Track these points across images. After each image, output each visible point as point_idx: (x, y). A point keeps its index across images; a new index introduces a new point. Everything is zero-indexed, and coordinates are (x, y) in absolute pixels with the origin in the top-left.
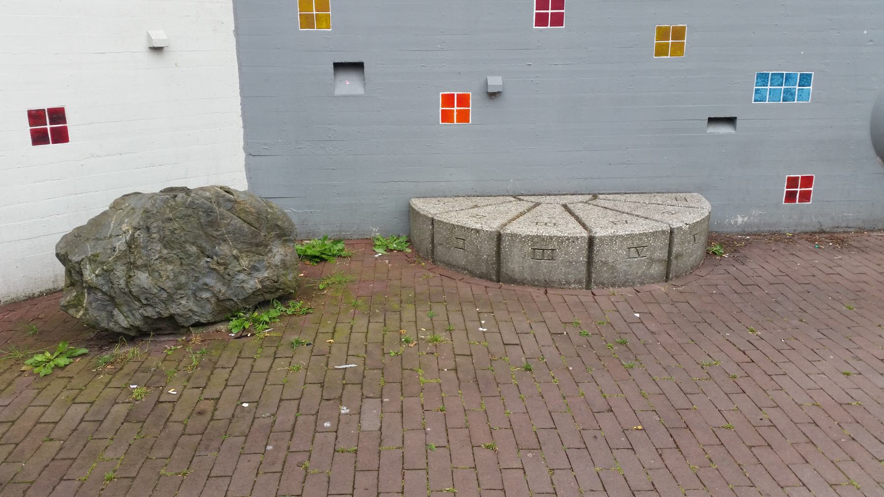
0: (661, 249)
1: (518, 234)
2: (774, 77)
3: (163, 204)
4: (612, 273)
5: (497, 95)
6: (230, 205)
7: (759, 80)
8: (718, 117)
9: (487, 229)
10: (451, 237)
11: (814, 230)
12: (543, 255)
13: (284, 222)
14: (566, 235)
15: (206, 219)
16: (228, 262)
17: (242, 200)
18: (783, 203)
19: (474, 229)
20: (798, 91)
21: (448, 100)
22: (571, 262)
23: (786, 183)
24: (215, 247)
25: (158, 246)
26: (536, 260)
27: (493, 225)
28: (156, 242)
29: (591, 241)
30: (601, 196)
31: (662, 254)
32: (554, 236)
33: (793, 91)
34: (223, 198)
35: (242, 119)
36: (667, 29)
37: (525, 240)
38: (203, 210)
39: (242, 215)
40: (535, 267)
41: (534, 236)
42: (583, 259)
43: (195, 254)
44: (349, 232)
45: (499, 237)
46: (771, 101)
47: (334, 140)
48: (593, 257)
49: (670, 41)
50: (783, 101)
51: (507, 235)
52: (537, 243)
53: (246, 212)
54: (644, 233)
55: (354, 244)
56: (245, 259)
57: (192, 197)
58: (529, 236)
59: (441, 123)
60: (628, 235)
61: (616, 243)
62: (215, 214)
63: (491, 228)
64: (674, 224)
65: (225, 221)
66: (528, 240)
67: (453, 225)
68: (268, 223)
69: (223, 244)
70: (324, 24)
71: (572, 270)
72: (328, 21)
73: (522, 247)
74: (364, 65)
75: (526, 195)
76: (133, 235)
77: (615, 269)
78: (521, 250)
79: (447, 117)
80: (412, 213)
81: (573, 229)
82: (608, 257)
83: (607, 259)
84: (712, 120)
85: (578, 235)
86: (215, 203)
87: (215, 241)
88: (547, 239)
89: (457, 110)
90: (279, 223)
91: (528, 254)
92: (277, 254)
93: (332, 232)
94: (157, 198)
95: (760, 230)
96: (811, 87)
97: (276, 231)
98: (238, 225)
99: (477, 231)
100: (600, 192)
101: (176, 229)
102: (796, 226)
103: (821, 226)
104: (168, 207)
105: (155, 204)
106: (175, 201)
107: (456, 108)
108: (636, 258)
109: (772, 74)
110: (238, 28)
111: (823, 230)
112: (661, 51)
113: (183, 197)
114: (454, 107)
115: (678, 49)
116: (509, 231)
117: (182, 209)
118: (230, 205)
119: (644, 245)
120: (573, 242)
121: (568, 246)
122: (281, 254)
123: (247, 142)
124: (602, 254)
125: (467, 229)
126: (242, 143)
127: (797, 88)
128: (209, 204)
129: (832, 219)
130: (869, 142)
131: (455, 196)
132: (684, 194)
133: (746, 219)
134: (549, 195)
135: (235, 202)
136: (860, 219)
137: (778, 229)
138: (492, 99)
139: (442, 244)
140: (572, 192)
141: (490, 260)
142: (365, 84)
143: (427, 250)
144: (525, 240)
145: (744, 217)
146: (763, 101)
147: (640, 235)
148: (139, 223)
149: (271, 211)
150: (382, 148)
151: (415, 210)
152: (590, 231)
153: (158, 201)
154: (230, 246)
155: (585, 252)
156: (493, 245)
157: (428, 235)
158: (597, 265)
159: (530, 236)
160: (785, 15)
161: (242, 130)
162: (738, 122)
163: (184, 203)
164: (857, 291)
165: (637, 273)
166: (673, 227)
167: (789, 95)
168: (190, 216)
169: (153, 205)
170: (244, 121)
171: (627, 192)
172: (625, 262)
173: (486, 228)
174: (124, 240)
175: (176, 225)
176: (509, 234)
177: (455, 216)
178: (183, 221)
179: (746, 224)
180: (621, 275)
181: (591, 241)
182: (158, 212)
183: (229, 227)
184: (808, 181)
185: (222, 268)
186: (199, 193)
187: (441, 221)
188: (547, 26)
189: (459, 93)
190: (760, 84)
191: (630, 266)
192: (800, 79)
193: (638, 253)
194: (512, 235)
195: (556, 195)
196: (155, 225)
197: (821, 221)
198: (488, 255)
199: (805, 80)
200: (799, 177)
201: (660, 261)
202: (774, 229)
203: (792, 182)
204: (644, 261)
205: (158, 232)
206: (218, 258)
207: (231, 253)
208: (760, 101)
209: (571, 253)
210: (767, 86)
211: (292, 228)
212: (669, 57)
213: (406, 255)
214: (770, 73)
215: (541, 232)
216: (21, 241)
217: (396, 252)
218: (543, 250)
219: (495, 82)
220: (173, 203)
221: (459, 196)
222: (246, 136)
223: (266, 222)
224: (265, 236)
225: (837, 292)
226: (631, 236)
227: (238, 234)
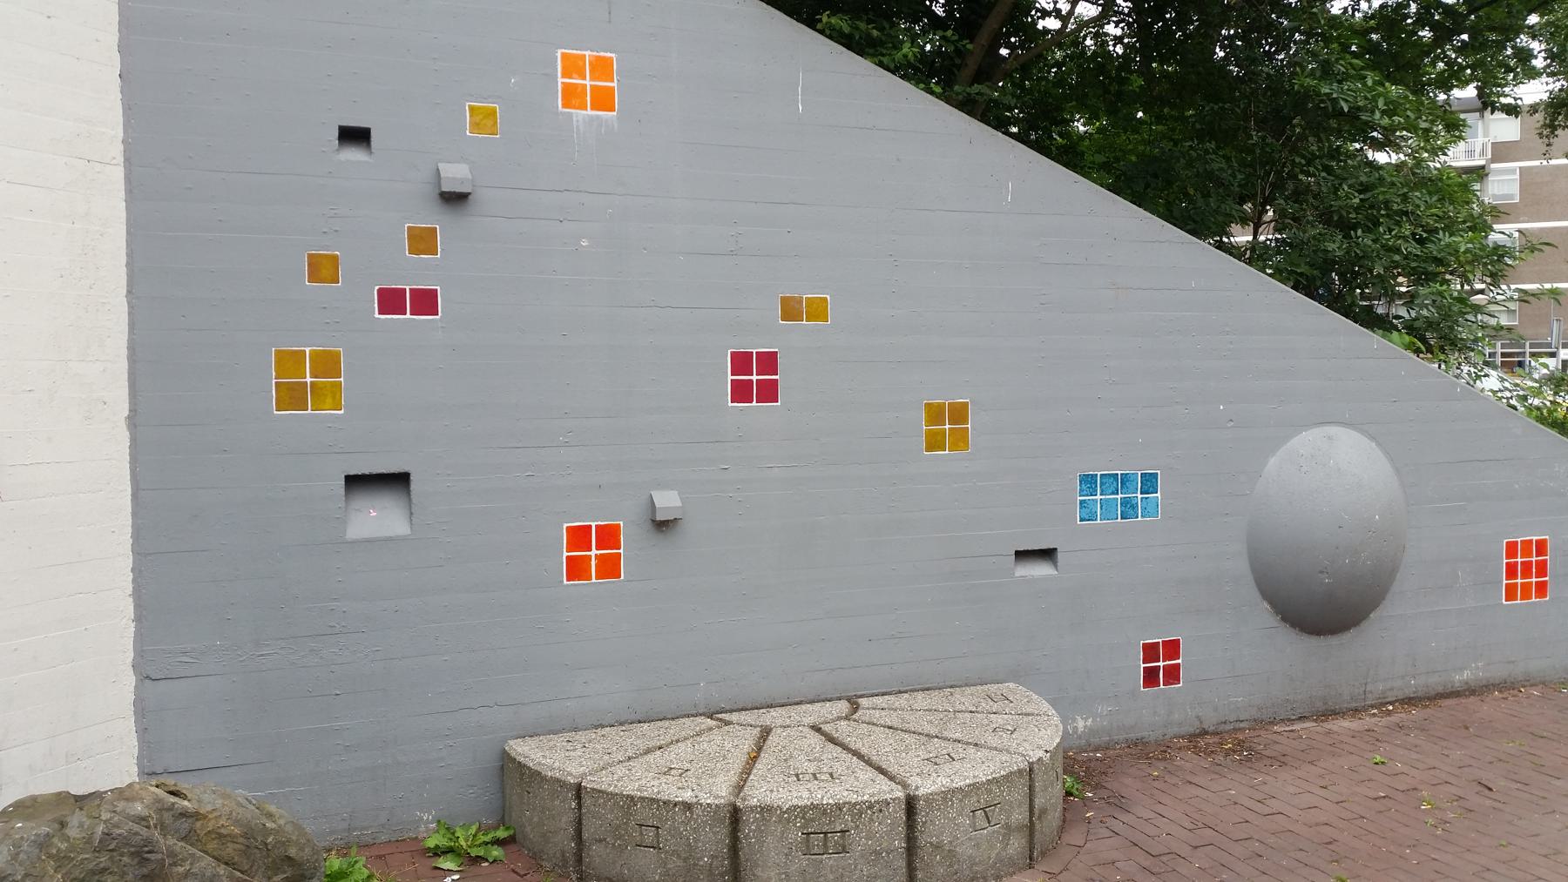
0: (1020, 806)
1: (775, 805)
2: (1104, 480)
3: (38, 850)
4: (951, 866)
5: (671, 525)
6: (184, 825)
7: (1083, 485)
8: (1030, 549)
9: (709, 801)
10: (625, 823)
11: (1191, 730)
12: (825, 845)
13: (302, 849)
14: (865, 798)
15: (137, 872)
17: (209, 808)
18: (1142, 689)
19: (679, 802)
20: (1142, 501)
21: (579, 537)
22: (878, 853)
23: (1142, 653)
26: (813, 857)
27: (717, 791)
29: (911, 805)
30: (864, 702)
31: (1019, 816)
32: (845, 803)
33: (1133, 502)
34: (172, 813)
35: (134, 601)
36: (941, 407)
37: (790, 818)
38: (133, 849)
39: (211, 846)
40: (811, 871)
41: (805, 807)
42: (899, 844)
44: (366, 828)
45: (735, 815)
46: (1104, 519)
47: (341, 633)
48: (916, 838)
49: (947, 426)
50: (1122, 519)
51: (753, 809)
52: (813, 820)
53: (220, 836)
54: (994, 778)
55: (384, 856)
57: (105, 822)
58: (796, 807)
59: (565, 582)
60: (969, 785)
61: (952, 804)
62: (159, 856)
63: (717, 797)
64: (1031, 753)
65: (181, 869)
66: (796, 817)
67: (632, 798)
68: (269, 856)
70: (329, 400)
71: (882, 869)
72: (338, 397)
73: (783, 833)
74: (411, 478)
75: (731, 711)
77: (954, 856)
78: (782, 837)
79: (576, 569)
80: (511, 772)
81: (864, 786)
82: (942, 833)
83: (941, 838)
84: (1022, 555)
85: (888, 796)
86: (156, 827)
88: (831, 811)
89: (596, 555)
90: (292, 852)
91: (796, 846)
93: (332, 832)
94: (22, 838)
95: (1113, 740)
96: (1159, 495)
97: (285, 872)
98: (208, 874)
99: (688, 806)
100: (859, 693)
102: (1166, 727)
103: (1201, 722)
104: (50, 856)
105: (18, 854)
106: (67, 839)
107: (594, 552)
108: (984, 829)
109: (1101, 475)
110: (136, 411)
111: (1204, 729)
112: (934, 443)
113: (81, 825)
114: (591, 550)
115: (960, 440)
116: (755, 800)
117: (87, 856)
119: (995, 802)
120: (881, 811)
121: (871, 820)
123: (143, 651)
124: (933, 828)
125: (665, 803)
126: (130, 656)
127: (1140, 496)
128: (144, 832)
129: (1216, 710)
130: (1249, 579)
131: (596, 727)
132: (996, 686)
133: (1089, 722)
134: (771, 706)
135: (197, 816)
136: (1254, 706)
137: (1139, 735)
138: (663, 531)
139: (605, 839)
140: (811, 697)
141: (718, 868)
142: (411, 514)
143: (563, 856)
144: (790, 818)
145: (1086, 720)
146: (1093, 520)
147: (988, 785)
149: (274, 826)
150: (446, 641)
151: (529, 768)
152: (905, 786)
153: (25, 847)
155: (901, 829)
156: (723, 832)
157: (566, 821)
158: (924, 853)
159: (799, 807)
160: (1111, 382)
161: (133, 625)
162: (1060, 556)
163: (89, 841)
164: (1327, 844)
165: (989, 858)
166: (1031, 760)
167: (1129, 508)
168: (103, 871)
169: (15, 857)
170: (138, 606)
171: (902, 689)
172: (970, 839)
173: (706, 799)
176: (756, 807)
177: (627, 775)
179: (1091, 731)
180: (965, 867)
181: (911, 805)
182: (27, 875)
184: (1172, 648)
186: (118, 809)
187: (600, 791)
188: (752, 402)
189: (600, 523)
190: (1085, 492)
191: (977, 845)
192: (1141, 483)
193: (988, 819)
194: (762, 809)
195: (783, 706)
197: (1200, 714)
198: (713, 857)
199: (1149, 483)
200: (1159, 643)
201: (1019, 828)
202: (1133, 736)
203: (1150, 652)
204: (998, 832)
208: (1089, 520)
209: (878, 835)
210: (1096, 495)
211: (316, 860)
212: (947, 452)
213: (513, 871)
214: (1099, 473)
215: (819, 796)
217: (486, 864)
218: (825, 833)
219: (667, 501)
220: (63, 846)
221: (603, 726)
222: (140, 638)
225: (1301, 850)
226: (975, 787)
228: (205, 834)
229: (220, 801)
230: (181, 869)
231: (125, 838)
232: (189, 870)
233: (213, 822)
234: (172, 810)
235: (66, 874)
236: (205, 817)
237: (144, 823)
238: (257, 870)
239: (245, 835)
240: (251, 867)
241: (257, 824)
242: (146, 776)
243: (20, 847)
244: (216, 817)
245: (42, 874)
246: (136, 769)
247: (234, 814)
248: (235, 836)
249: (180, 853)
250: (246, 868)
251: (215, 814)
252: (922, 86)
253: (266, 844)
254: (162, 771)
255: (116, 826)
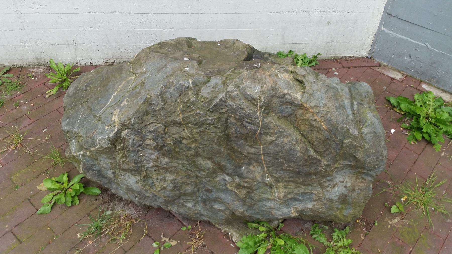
3: (178, 95)
16: (255, 188)
24: (240, 167)
25: (153, 154)
28: (151, 149)
34: (281, 100)
38: (237, 117)
39: (303, 128)
43: (208, 170)
56: (281, 190)
62: (254, 127)
69: (254, 164)
76: (119, 132)
87: (244, 159)
92: (340, 184)
97: (350, 162)
101: (184, 138)
117: (201, 113)
118: (289, 110)
122: (345, 187)
148: (130, 119)
154: (264, 171)
174: (107, 137)
175: (186, 133)
178: (199, 130)
183: (271, 147)
185: (244, 192)
196: (152, 129)
205: (155, 139)
206: (242, 180)
207: (263, 179)
216: (131, 14)
220: (193, 99)
223: (339, 147)
224: (327, 166)
227: (281, 157)
228: (302, 119)
229: (324, 102)
230: (269, 138)
231: (233, 108)
232: (274, 141)
233: (310, 115)
234: (282, 98)
235: (185, 117)
236: (306, 109)
237: (254, 102)
238: (329, 154)
239: (329, 131)
240: (325, 151)
241: (343, 127)
242: (387, 14)
243: (169, 88)
244: (313, 112)
245: (173, 111)
246: (383, 9)
247: (329, 115)
248: (323, 130)
249: (272, 129)
250: (320, 150)
251: (314, 110)
252: (174, 43)
253: (343, 142)
254: (395, 15)
255: (233, 99)
